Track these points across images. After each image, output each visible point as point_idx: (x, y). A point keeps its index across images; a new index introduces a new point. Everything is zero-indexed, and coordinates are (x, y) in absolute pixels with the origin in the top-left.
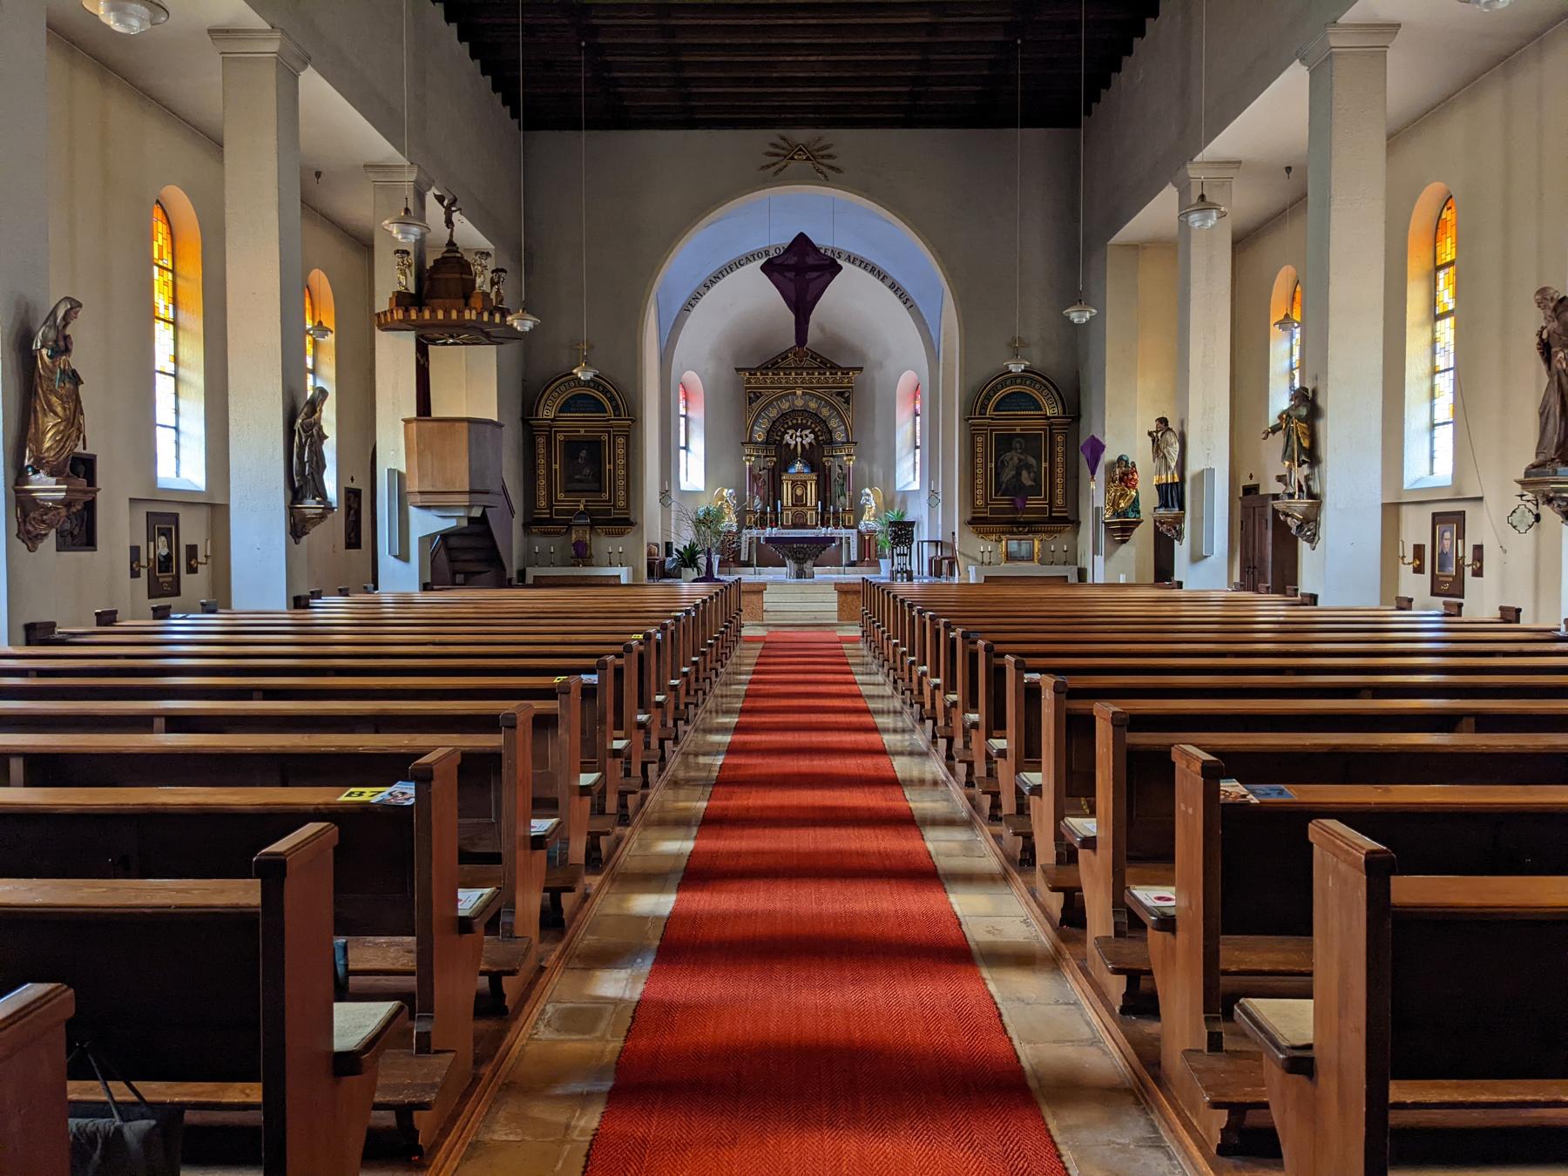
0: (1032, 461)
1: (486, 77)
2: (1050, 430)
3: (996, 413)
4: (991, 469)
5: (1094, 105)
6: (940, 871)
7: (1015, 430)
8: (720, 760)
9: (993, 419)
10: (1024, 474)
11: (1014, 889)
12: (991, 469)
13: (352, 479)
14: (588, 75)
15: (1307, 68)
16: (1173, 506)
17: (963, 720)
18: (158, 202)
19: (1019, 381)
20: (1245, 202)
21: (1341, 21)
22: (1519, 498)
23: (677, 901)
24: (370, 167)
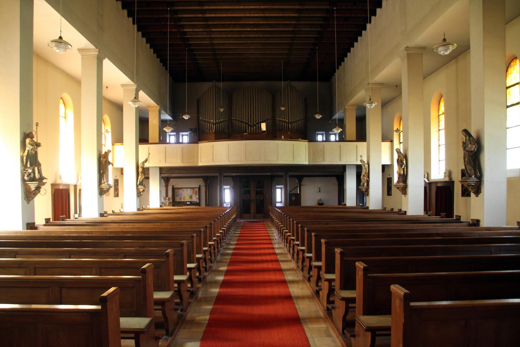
5: (340, 66)
6: (287, 281)
8: (230, 257)
11: (292, 262)
13: (116, 176)
14: (189, 57)
17: (297, 248)
18: (61, 98)
23: (227, 268)
24: (122, 85)
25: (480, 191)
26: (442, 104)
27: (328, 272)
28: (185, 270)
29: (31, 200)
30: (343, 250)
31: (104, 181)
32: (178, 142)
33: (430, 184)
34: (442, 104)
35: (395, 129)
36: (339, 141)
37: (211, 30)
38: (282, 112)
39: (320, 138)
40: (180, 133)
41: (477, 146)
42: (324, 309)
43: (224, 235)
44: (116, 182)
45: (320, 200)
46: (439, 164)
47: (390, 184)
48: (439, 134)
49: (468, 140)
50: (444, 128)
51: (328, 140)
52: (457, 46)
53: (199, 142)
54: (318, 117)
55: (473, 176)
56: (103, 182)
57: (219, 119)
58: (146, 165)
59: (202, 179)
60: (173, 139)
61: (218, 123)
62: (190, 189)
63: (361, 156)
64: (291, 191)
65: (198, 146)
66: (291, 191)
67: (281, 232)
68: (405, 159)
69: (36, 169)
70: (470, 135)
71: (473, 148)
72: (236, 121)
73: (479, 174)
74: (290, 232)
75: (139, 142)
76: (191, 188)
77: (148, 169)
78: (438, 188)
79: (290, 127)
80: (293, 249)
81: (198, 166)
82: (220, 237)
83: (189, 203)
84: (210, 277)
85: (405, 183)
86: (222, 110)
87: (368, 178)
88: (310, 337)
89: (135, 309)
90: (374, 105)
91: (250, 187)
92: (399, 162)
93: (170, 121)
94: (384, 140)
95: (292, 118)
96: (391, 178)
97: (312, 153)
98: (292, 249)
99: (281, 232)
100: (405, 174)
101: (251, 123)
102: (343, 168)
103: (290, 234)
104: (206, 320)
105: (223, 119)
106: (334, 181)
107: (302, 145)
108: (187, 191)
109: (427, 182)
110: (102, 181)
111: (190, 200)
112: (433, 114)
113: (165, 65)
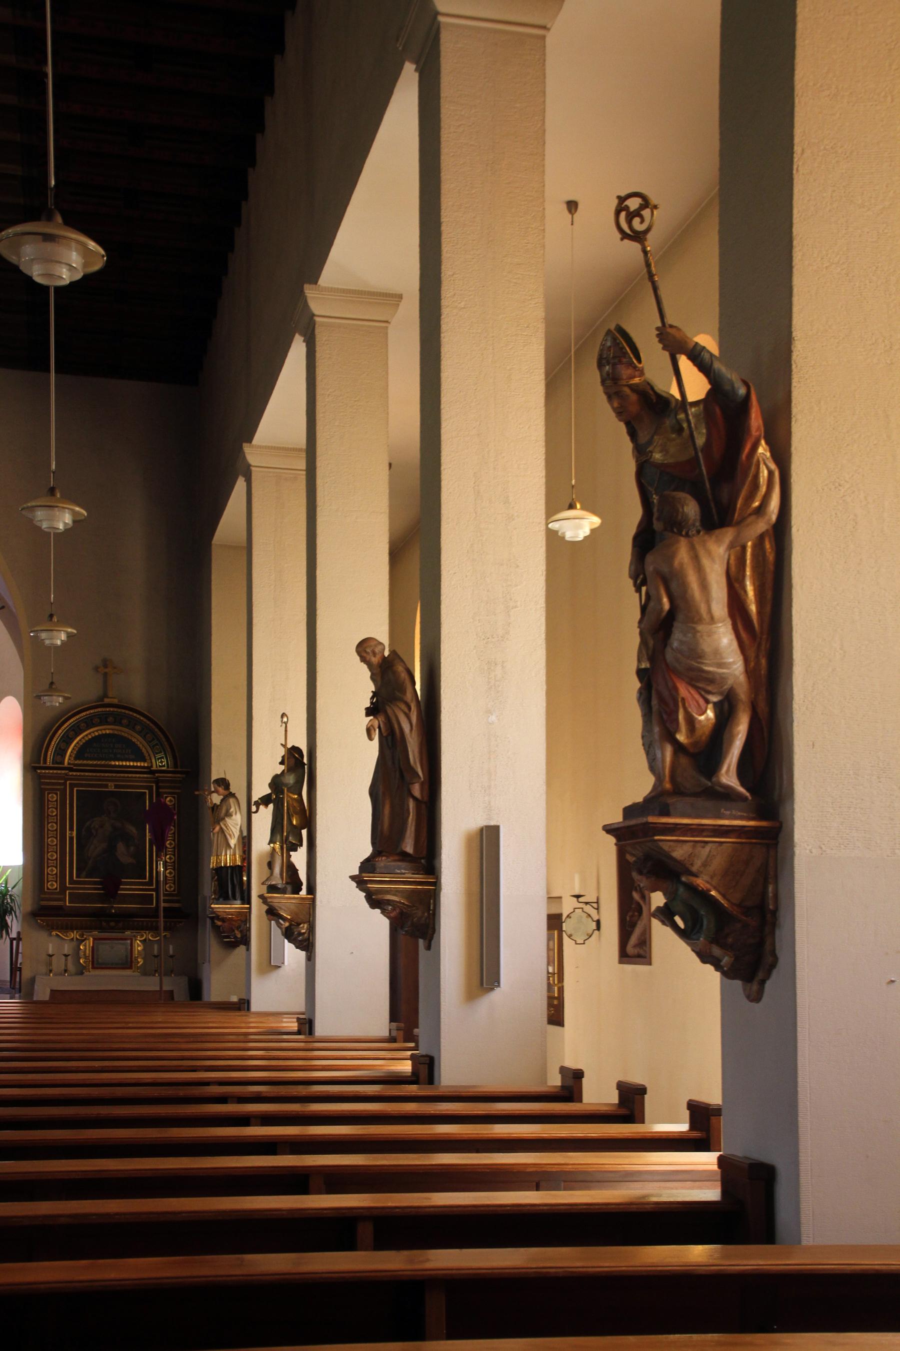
0: (132, 830)
2: (158, 788)
3: (77, 762)
4: (71, 839)
7: (106, 786)
9: (71, 770)
10: (121, 847)
12: (71, 839)
16: (235, 899)
19: (110, 719)
22: (575, 899)
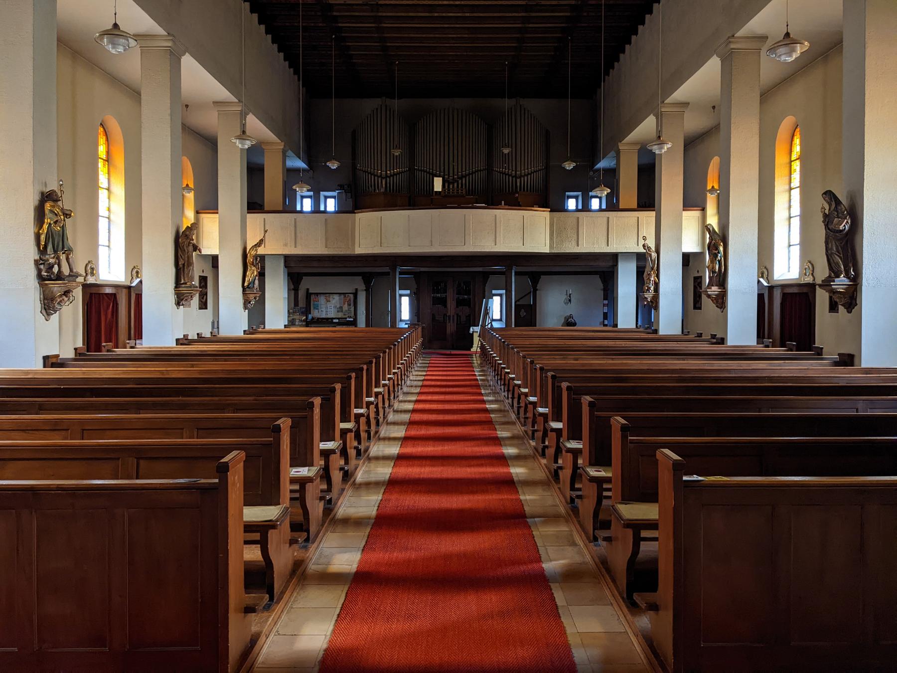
1: (280, 53)
13: (203, 271)
15: (719, 59)
20: (693, 123)
21: (737, 35)
24: (216, 103)
25: (854, 302)
26: (797, 141)
27: (571, 437)
28: (316, 454)
29: (52, 314)
30: (593, 400)
31: (184, 280)
32: (316, 210)
33: (771, 288)
34: (797, 141)
35: (709, 187)
36: (608, 209)
37: (377, 3)
38: (504, 155)
39: (571, 204)
40: (321, 193)
41: (849, 221)
42: (566, 502)
43: (396, 383)
44: (203, 280)
45: (571, 316)
46: (789, 252)
47: (698, 288)
48: (790, 196)
49: (834, 210)
50: (798, 185)
51: (586, 208)
52: (809, 45)
53: (355, 211)
54: (569, 166)
55: (842, 276)
56: (182, 282)
57: (392, 169)
58: (261, 251)
59: (361, 277)
60: (307, 205)
61: (391, 175)
62: (338, 295)
63: (645, 238)
64: (518, 300)
65: (355, 216)
66: (518, 300)
67: (503, 377)
68: (722, 244)
69: (63, 257)
70: (838, 202)
71: (843, 225)
72: (423, 173)
73: (853, 271)
74: (547, 401)
75: (249, 208)
76: (340, 294)
77: (262, 258)
78: (785, 296)
79: (518, 184)
80: (519, 403)
81: (355, 254)
82: (394, 380)
83: (337, 321)
84: (375, 449)
85: (722, 287)
86: (397, 153)
87: (656, 278)
88: (540, 546)
89: (260, 493)
90: (666, 148)
91: (445, 292)
92: (711, 249)
93: (304, 170)
94: (688, 205)
95: (523, 169)
96: (701, 277)
97: (555, 232)
98: (517, 403)
99: (503, 377)
100: (723, 270)
101: (449, 177)
102: (614, 258)
103: (505, 366)
104: (386, 474)
105: (402, 169)
106: (597, 281)
107: (541, 218)
108: (334, 299)
109: (765, 284)
110: (181, 281)
111: (340, 315)
112: (780, 159)
113: (296, 72)
